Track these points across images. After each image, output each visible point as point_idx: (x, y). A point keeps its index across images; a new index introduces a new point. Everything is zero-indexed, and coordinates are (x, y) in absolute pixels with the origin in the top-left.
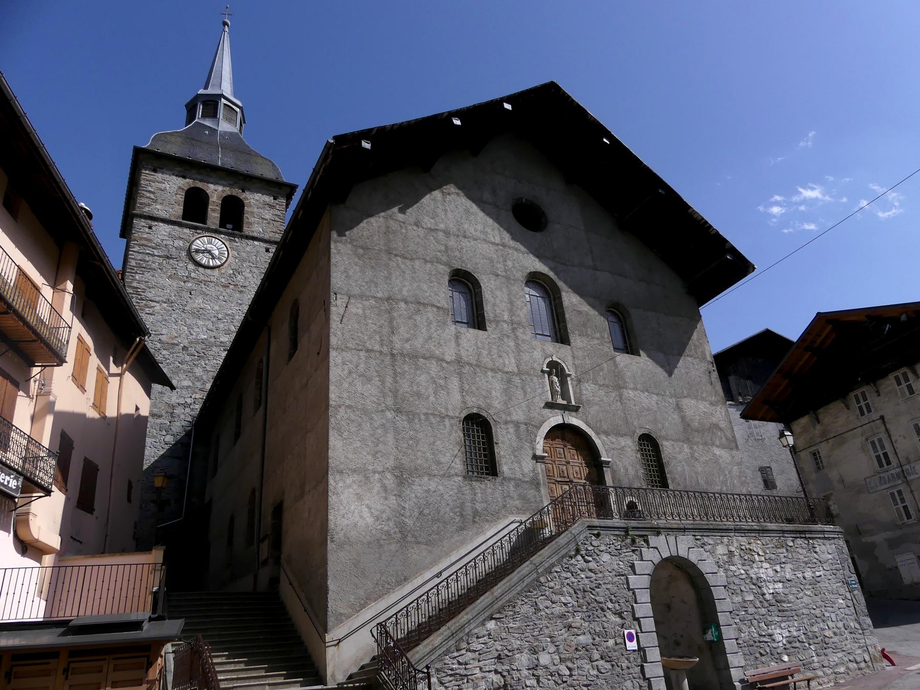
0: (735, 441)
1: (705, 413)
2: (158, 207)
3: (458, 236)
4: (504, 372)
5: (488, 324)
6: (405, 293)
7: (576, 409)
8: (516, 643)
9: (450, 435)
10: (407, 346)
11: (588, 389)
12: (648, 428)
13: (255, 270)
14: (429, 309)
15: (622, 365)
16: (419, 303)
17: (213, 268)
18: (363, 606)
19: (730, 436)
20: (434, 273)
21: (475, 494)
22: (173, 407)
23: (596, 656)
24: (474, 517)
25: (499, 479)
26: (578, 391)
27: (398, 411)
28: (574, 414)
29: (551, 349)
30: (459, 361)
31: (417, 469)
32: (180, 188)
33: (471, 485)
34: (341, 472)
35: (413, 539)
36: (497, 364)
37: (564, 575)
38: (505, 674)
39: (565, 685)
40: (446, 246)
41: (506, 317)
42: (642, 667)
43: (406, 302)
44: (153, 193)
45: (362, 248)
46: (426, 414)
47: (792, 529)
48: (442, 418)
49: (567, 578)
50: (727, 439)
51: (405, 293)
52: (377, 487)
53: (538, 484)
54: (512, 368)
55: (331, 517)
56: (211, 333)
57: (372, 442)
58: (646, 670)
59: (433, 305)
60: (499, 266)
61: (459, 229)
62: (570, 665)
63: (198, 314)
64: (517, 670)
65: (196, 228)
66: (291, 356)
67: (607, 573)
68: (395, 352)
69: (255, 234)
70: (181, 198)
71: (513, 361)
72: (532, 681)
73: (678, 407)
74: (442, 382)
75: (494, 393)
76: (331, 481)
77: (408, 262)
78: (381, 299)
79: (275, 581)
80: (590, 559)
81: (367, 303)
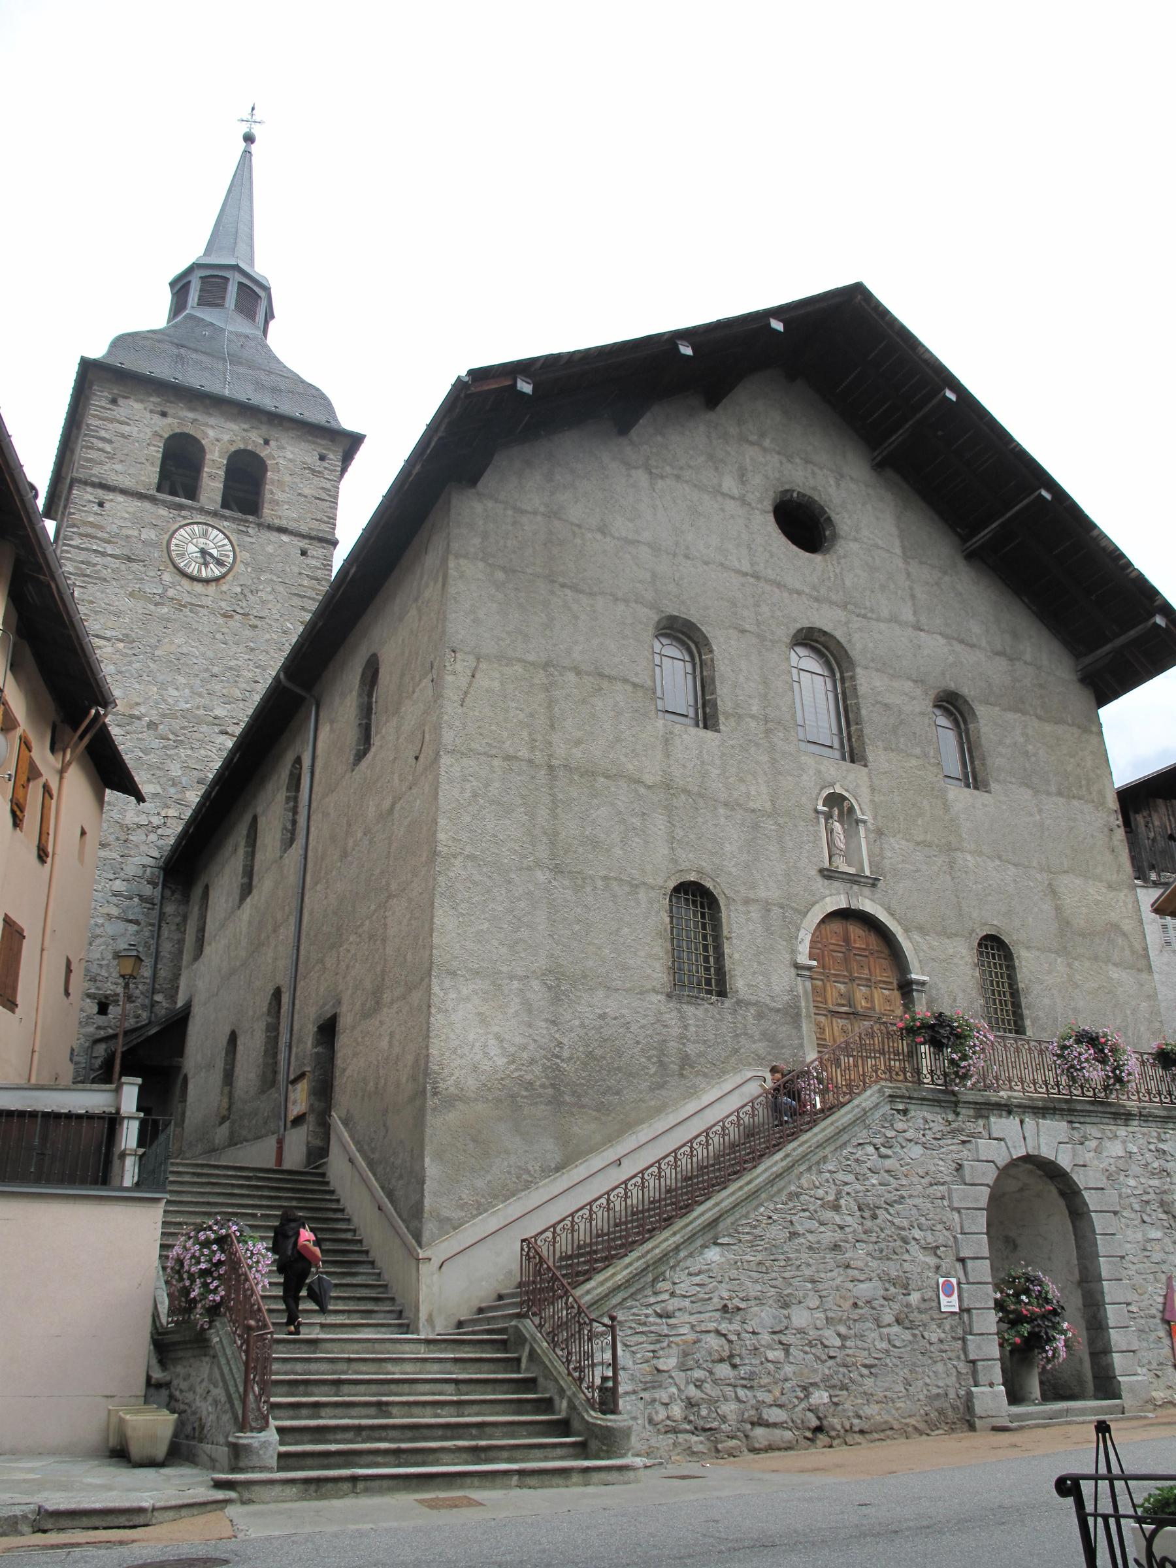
0: (1147, 957)
1: (1097, 903)
2: (118, 467)
3: (675, 555)
4: (746, 810)
5: (722, 719)
6: (575, 655)
7: (874, 883)
8: (753, 1289)
9: (646, 918)
10: (577, 752)
11: (895, 846)
12: (993, 920)
13: (281, 588)
14: (619, 686)
16: (601, 675)
17: (207, 581)
18: (481, 1209)
19: (1138, 946)
20: (629, 621)
21: (686, 1027)
22: (127, 829)
23: (888, 1318)
24: (682, 1068)
25: (728, 1003)
26: (877, 851)
27: (558, 870)
28: (867, 891)
29: (832, 771)
30: (667, 785)
31: (585, 977)
32: (156, 434)
33: (679, 1011)
34: (454, 974)
35: (574, 1100)
36: (736, 794)
37: (840, 1176)
38: (734, 1338)
39: (831, 1363)
40: (654, 575)
41: (755, 709)
42: (964, 1340)
43: (578, 672)
45: (503, 569)
46: (605, 878)
47: (309, 775)
49: (846, 1184)
50: (1133, 952)
51: (575, 655)
52: (515, 1005)
53: (798, 1015)
54: (761, 802)
55: (433, 1051)
56: (198, 700)
57: (510, 923)
58: (971, 1347)
59: (625, 681)
60: (746, 613)
61: (677, 544)
62: (843, 1330)
63: (177, 663)
64: (754, 1333)
65: (181, 507)
66: (360, 756)
67: (916, 1180)
68: (554, 762)
69: (284, 523)
71: (764, 789)
72: (776, 1353)
74: (636, 822)
75: (727, 847)
76: (436, 989)
77: (584, 599)
78: (532, 664)
79: (318, 1153)
80: (889, 1152)
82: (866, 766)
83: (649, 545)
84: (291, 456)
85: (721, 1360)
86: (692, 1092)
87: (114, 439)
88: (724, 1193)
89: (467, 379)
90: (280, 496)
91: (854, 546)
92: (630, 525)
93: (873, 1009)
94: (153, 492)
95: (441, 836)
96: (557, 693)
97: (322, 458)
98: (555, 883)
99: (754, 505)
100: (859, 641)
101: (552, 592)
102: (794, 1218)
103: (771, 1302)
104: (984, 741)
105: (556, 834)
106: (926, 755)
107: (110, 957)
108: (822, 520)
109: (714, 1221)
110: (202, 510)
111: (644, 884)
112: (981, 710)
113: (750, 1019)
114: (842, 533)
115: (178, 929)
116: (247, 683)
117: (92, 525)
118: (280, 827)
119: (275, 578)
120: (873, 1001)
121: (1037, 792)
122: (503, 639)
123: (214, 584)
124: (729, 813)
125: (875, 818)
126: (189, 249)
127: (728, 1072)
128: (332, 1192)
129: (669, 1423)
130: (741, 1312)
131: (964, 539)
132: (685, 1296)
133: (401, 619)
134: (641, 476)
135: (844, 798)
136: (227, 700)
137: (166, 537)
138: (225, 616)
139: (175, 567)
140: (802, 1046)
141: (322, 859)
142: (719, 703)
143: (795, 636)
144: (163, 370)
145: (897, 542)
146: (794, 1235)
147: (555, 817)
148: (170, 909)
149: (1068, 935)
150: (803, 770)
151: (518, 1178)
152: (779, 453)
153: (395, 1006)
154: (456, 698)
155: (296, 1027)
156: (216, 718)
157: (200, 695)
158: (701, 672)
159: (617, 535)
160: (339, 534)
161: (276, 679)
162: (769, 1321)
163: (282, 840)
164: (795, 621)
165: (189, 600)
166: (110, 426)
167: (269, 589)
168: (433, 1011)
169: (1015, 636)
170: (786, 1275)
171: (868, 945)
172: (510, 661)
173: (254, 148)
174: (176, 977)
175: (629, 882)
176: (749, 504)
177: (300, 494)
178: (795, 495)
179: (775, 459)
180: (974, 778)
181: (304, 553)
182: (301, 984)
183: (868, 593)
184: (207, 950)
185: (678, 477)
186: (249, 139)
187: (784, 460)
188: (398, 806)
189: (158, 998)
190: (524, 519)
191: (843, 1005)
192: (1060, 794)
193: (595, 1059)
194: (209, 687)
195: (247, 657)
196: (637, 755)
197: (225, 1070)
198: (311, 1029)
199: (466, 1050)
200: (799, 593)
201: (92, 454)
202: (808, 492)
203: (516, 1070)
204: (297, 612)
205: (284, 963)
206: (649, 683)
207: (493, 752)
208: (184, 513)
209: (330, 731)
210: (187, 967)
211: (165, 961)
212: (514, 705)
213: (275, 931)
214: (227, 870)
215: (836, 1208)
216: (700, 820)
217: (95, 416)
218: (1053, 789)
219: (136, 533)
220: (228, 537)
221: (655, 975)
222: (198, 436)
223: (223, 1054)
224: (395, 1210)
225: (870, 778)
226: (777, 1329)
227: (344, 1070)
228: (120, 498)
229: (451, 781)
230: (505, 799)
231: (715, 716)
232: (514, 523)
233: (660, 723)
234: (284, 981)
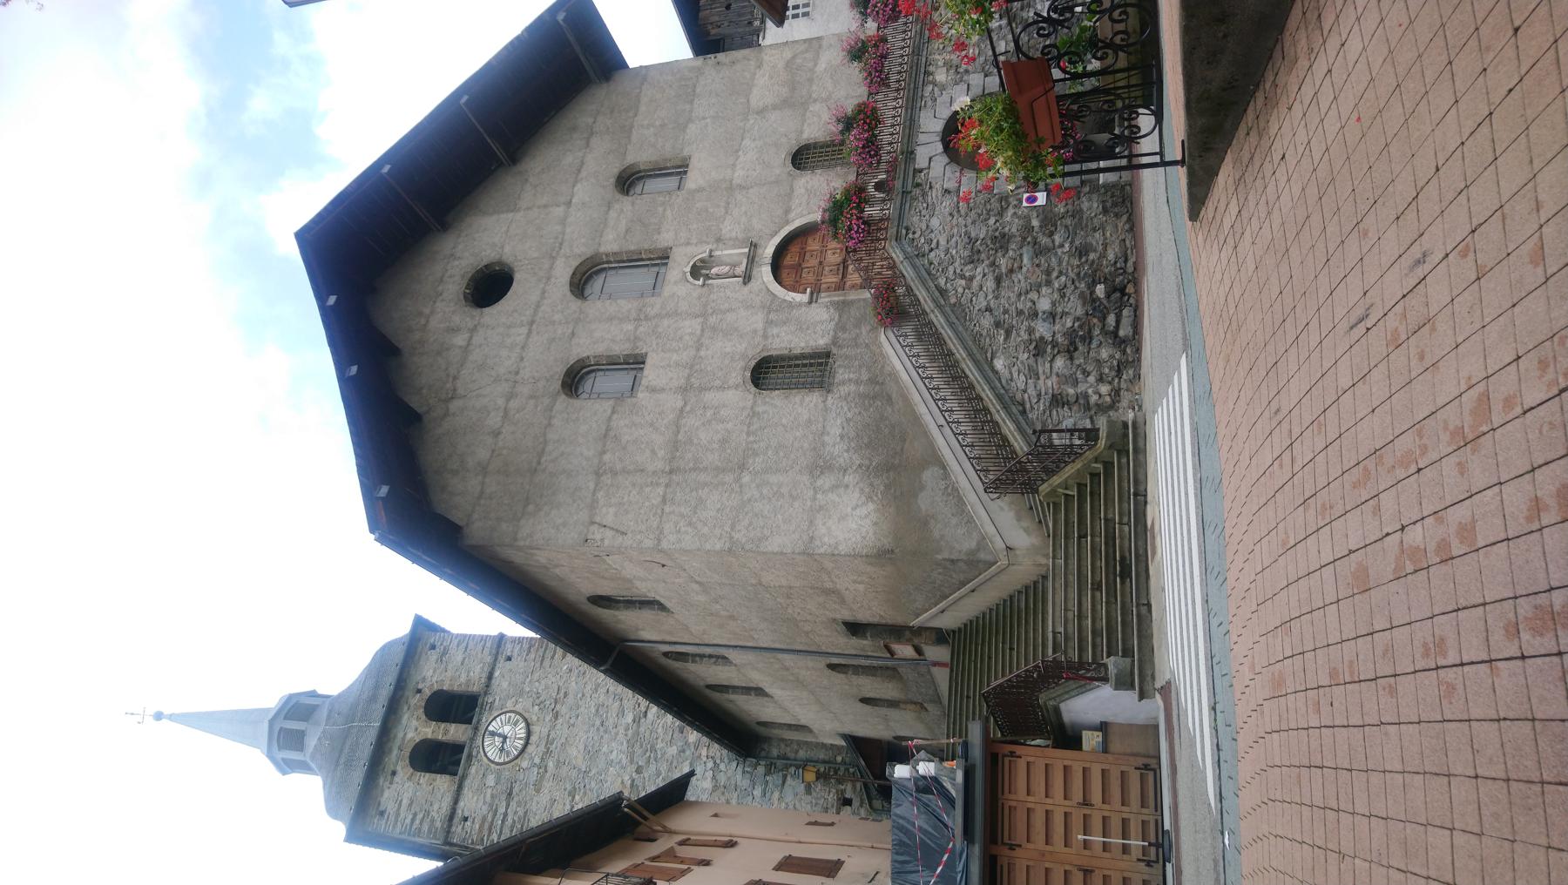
7: (754, 246)
10: (661, 453)
11: (729, 229)
13: (536, 676)
14: (613, 424)
15: (701, 182)
18: (970, 521)
19: (803, 47)
22: (715, 788)
25: (834, 350)
27: (742, 467)
28: (760, 251)
30: (685, 390)
40: (531, 397)
43: (604, 452)
44: (415, 815)
46: (748, 434)
48: (754, 414)
52: (832, 497)
53: (844, 302)
62: (1055, 274)
63: (591, 753)
65: (470, 756)
66: (662, 607)
69: (484, 675)
70: (425, 778)
71: (687, 323)
73: (761, 112)
74: (709, 413)
76: (822, 551)
77: (549, 448)
79: (941, 636)
81: (601, 502)
83: (508, 400)
90: (463, 679)
91: (507, 249)
95: (718, 547)
97: (433, 647)
100: (579, 248)
104: (654, 158)
105: (717, 468)
106: (663, 204)
110: (472, 739)
112: (631, 159)
117: (481, 826)
121: (690, 120)
126: (254, 761)
131: (500, 164)
133: (562, 580)
134: (455, 405)
135: (694, 266)
136: (621, 713)
146: (989, 309)
148: (775, 752)
149: (793, 101)
160: (494, 633)
161: (604, 672)
169: (574, 129)
172: (595, 501)
173: (166, 712)
174: (824, 746)
180: (679, 169)
181: (509, 659)
182: (824, 649)
184: (803, 722)
185: (455, 378)
186: (159, 716)
189: (839, 759)
192: (691, 102)
198: (854, 641)
200: (544, 292)
202: (465, 281)
205: (810, 662)
209: (644, 629)
214: (746, 707)
215: (971, 279)
218: (688, 107)
222: (412, 745)
228: (461, 804)
229: (679, 541)
231: (636, 356)
233: (640, 395)
234: (821, 663)
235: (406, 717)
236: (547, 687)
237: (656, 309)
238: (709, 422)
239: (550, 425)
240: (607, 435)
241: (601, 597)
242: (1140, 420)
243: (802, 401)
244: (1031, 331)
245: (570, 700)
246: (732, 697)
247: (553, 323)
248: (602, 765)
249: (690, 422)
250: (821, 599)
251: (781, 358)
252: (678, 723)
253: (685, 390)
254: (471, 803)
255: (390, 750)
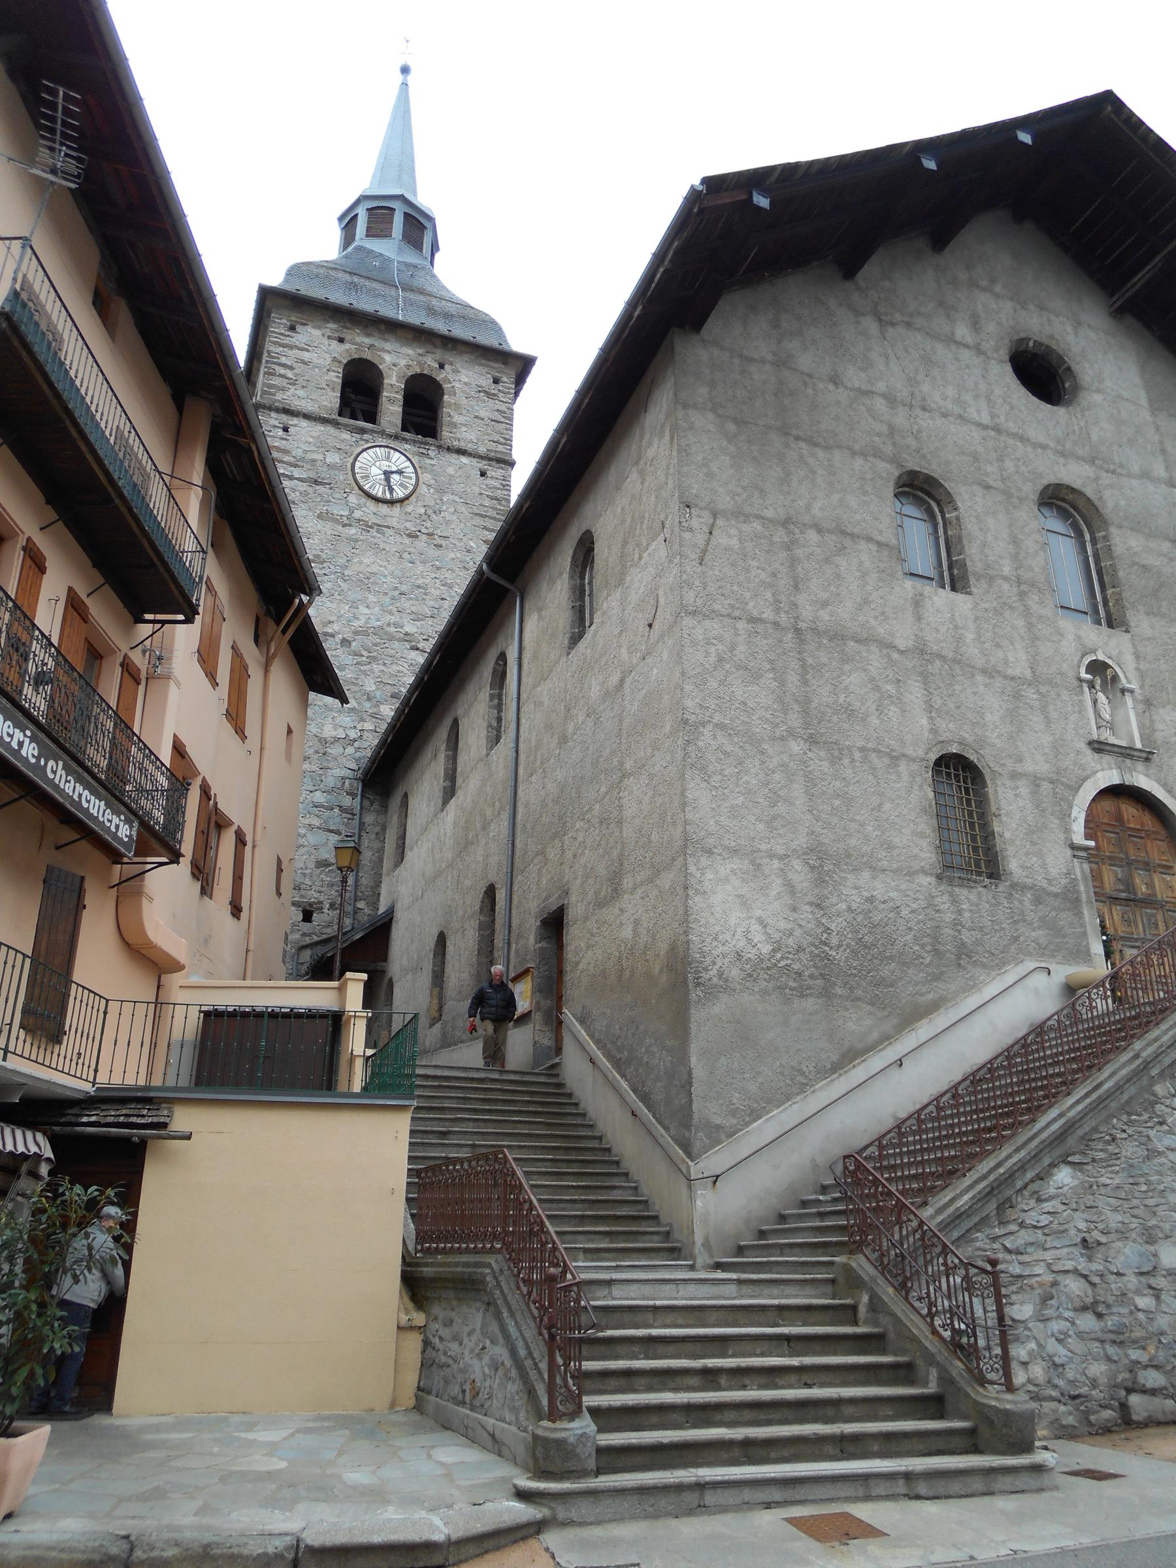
3: (911, 407)
4: (1006, 677)
5: (972, 580)
6: (816, 511)
8: (1114, 1220)
9: (909, 792)
10: (824, 615)
14: (862, 545)
18: (755, 1115)
20: (869, 476)
21: (960, 912)
22: (324, 742)
26: (1147, 723)
27: (812, 741)
28: (1140, 766)
30: (921, 650)
31: (849, 856)
32: (334, 359)
33: (951, 895)
34: (710, 852)
38: (1096, 1280)
41: (1007, 570)
43: (820, 531)
45: (734, 420)
46: (863, 749)
48: (895, 759)
52: (777, 886)
56: (388, 618)
57: (766, 797)
59: (869, 539)
60: (989, 469)
63: (366, 582)
64: (1118, 1274)
65: (363, 431)
66: (576, 639)
69: (462, 445)
71: (1023, 656)
75: (989, 717)
76: (692, 869)
77: (820, 454)
78: (770, 520)
82: (1127, 631)
83: (884, 396)
84: (466, 380)
85: (1084, 1308)
86: (971, 987)
87: (295, 365)
88: (1070, 1101)
89: (700, 188)
90: (457, 418)
91: (1098, 398)
92: (863, 375)
93: (1155, 895)
94: (335, 416)
96: (799, 552)
97: (496, 381)
98: (810, 754)
99: (989, 354)
100: (1113, 498)
101: (787, 446)
102: (1152, 1133)
103: (1134, 1235)
105: (808, 701)
107: (313, 866)
108: (1061, 371)
109: (1061, 1134)
110: (383, 433)
111: (904, 755)
113: (1027, 903)
114: (1083, 383)
115: (377, 838)
116: (435, 600)
118: (485, 725)
119: (457, 499)
120: (1153, 888)
122: (739, 495)
123: (398, 505)
124: (988, 681)
125: (1142, 687)
126: (357, 180)
127: (1009, 963)
128: (570, 1095)
129: (1031, 1388)
130: (1101, 1248)
132: (1035, 1227)
133: (618, 488)
134: (870, 324)
135: (1105, 666)
136: (417, 618)
137: (351, 460)
138: (410, 536)
139: (361, 488)
140: (1085, 934)
141: (537, 749)
142: (968, 563)
143: (1042, 493)
144: (339, 297)
145: (1143, 394)
147: (805, 683)
148: (369, 819)
150: (1062, 635)
151: (792, 1080)
152: (1011, 299)
153: (640, 891)
154: (694, 556)
155: (514, 924)
156: (406, 634)
157: (391, 613)
158: (945, 532)
159: (849, 385)
160: (515, 455)
161: (480, 572)
162: (1135, 1260)
163: (488, 737)
164: (1041, 476)
165: (375, 521)
166: (290, 353)
167: (452, 510)
168: (690, 893)
170: (1151, 1202)
171: (1142, 825)
172: (747, 518)
173: (411, 79)
174: (378, 884)
175: (889, 754)
176: (984, 354)
177: (476, 417)
178: (1031, 344)
179: (1008, 305)
181: (483, 474)
182: (519, 878)
183: (1115, 448)
184: (409, 855)
185: (909, 325)
186: (405, 70)
187: (1018, 307)
188: (628, 681)
189: (361, 905)
190: (752, 368)
191: (1122, 891)
193: (866, 947)
194: (398, 604)
195: (433, 575)
196: (887, 618)
197: (434, 971)
199: (728, 936)
200: (1044, 447)
201: (276, 381)
202: (1046, 341)
203: (782, 958)
204: (479, 531)
206: (894, 541)
207: (737, 613)
208: (365, 436)
210: (388, 874)
211: (366, 869)
212: (755, 564)
213: (484, 829)
214: (428, 775)
216: (958, 687)
217: (275, 343)
219: (321, 457)
220: (409, 459)
221: (922, 855)
223: (432, 956)
224: (654, 1116)
225: (1133, 645)
226: (1145, 1269)
227: (578, 963)
228: (304, 423)
229: (694, 644)
230: (752, 664)
231: (965, 577)
232: (743, 372)
234: (497, 876)
235: (411, 352)
236: (448, 522)
237: (1035, 608)
238: (877, 688)
239: (854, 453)
240: (844, 534)
241: (591, 550)
242: (1046, 1480)
243: (921, 835)
244: (1123, 1234)
245: (433, 552)
246: (442, 757)
247: (1000, 459)
248: (352, 596)
249: (875, 659)
250: (602, 871)
251: (982, 801)
252: (404, 691)
253: (922, 652)
254: (304, 435)
255: (368, 335)
